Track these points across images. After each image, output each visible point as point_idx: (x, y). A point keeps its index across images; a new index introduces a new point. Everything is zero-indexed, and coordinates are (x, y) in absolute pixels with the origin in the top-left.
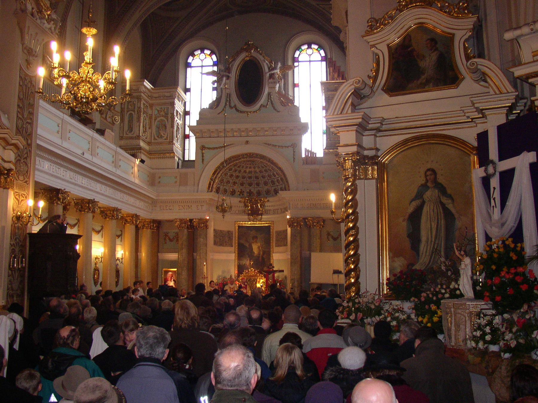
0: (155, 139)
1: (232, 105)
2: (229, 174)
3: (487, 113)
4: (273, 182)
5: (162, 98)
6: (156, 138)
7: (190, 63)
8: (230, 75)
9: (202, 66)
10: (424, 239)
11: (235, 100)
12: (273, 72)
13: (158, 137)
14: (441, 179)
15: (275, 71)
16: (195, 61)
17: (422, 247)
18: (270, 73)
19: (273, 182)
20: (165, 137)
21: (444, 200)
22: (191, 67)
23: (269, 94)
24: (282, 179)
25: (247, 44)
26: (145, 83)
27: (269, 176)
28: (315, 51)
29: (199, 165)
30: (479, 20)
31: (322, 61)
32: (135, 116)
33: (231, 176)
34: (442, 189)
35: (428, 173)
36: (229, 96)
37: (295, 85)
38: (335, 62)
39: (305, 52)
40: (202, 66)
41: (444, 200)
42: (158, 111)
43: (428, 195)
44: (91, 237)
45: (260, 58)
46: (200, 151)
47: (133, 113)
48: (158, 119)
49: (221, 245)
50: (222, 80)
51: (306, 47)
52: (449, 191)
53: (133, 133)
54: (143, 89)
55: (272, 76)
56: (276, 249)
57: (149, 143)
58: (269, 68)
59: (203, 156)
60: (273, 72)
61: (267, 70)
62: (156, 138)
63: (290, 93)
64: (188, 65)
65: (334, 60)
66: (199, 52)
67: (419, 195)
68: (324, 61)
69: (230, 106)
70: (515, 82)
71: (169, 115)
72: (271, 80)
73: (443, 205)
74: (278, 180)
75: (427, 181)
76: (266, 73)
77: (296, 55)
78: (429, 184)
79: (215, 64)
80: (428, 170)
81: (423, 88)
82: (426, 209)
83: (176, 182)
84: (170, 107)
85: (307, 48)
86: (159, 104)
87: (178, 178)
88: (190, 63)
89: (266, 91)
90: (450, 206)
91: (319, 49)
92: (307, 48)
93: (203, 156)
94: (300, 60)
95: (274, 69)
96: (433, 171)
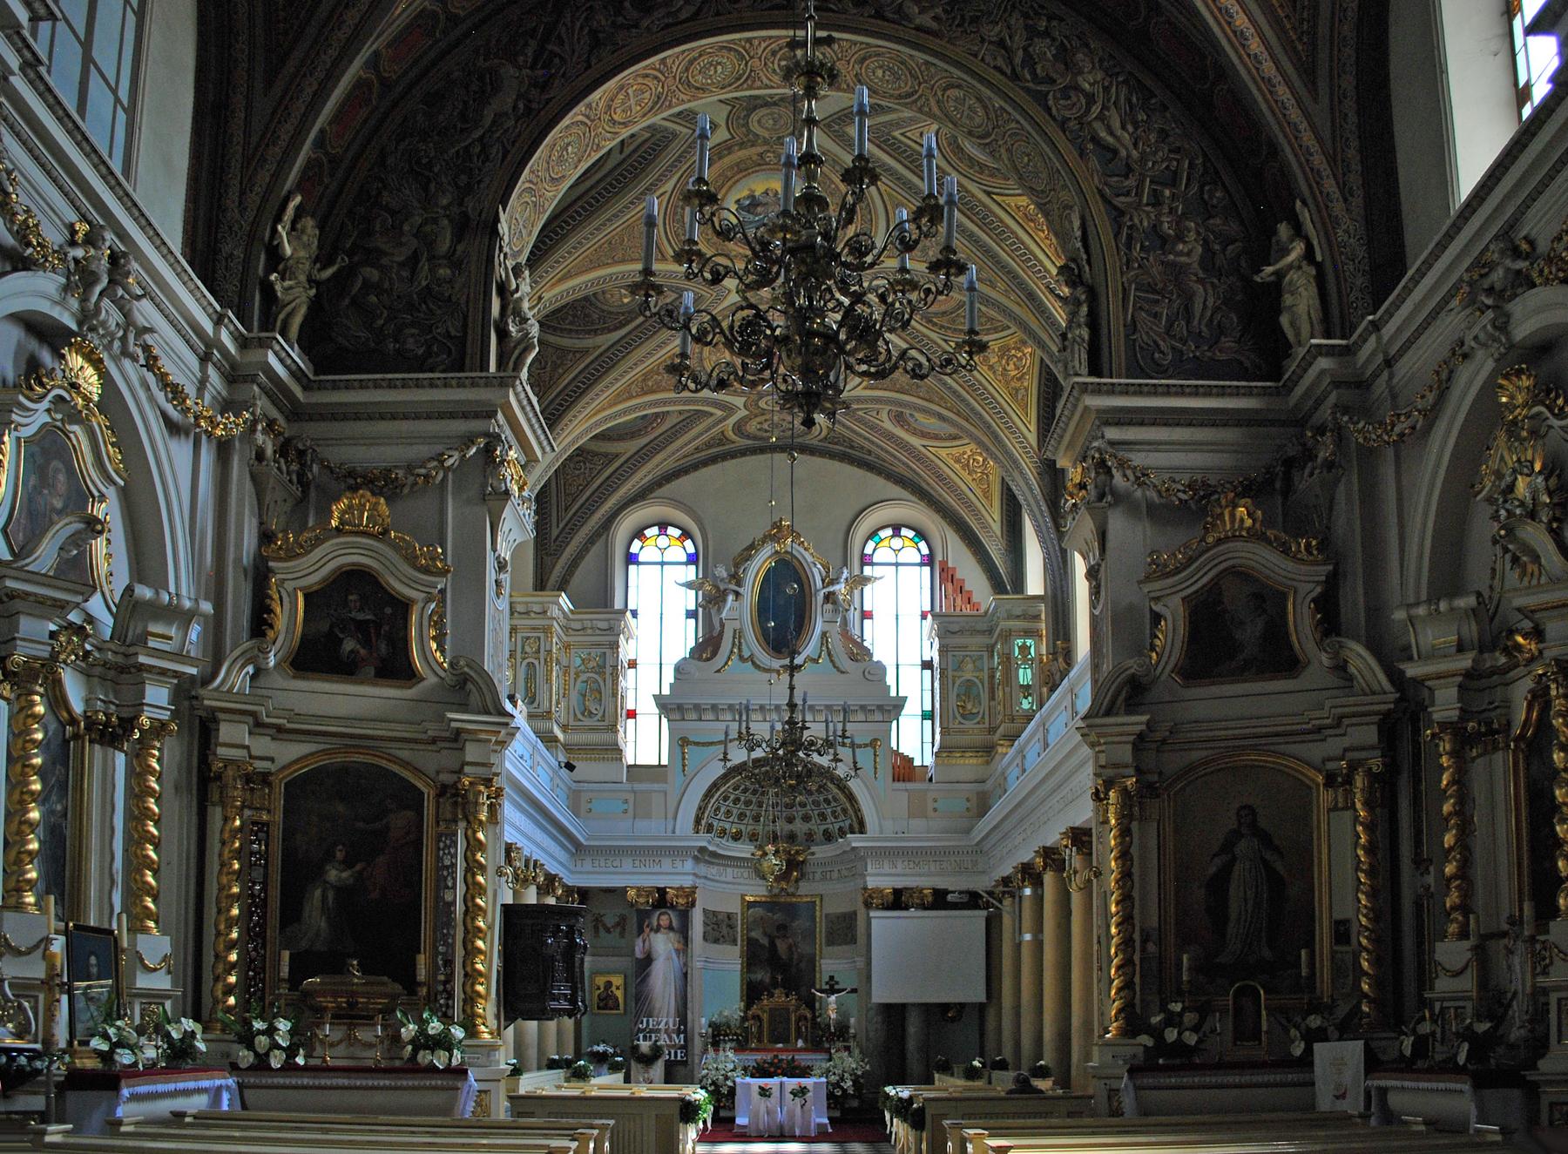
0: (576, 719)
1: (746, 654)
2: (732, 797)
3: (1499, 757)
4: (823, 816)
5: (589, 631)
6: (580, 716)
7: (636, 556)
8: (741, 590)
9: (662, 564)
10: (1233, 915)
11: (752, 643)
12: (831, 589)
13: (583, 714)
14: (1263, 823)
15: (836, 588)
16: (647, 551)
17: (1231, 929)
18: (826, 590)
19: (823, 816)
20: (598, 717)
21: (1268, 856)
22: (638, 563)
23: (824, 635)
24: (845, 811)
25: (777, 525)
26: (561, 600)
27: (813, 802)
28: (908, 543)
29: (676, 780)
30: (1336, 565)
31: (921, 564)
32: (540, 670)
33: (737, 800)
34: (1266, 839)
35: (1243, 813)
36: (738, 635)
37: (866, 615)
38: (954, 569)
39: (886, 543)
40: (662, 564)
41: (1268, 856)
42: (583, 660)
43: (1242, 847)
44: (527, 905)
45: (798, 551)
46: (678, 750)
47: (536, 662)
48: (583, 677)
49: (716, 941)
50: (725, 601)
51: (889, 532)
52: (1277, 842)
53: (535, 705)
54: (555, 612)
55: (829, 597)
56: (827, 950)
57: (564, 728)
58: (823, 581)
59: (684, 759)
60: (831, 589)
61: (819, 584)
62: (580, 716)
63: (857, 632)
64: (631, 559)
65: (950, 565)
66: (655, 530)
67: (1228, 846)
68: (925, 565)
69: (741, 657)
70: (1396, 677)
71: (608, 670)
72: (829, 606)
73: (1264, 861)
74: (834, 812)
75: (1240, 824)
76: (817, 591)
77: (868, 550)
78: (1244, 830)
79: (692, 559)
80: (1244, 807)
81: (1242, 672)
82: (1238, 868)
83: (625, 811)
84: (608, 652)
85: (892, 537)
86: (583, 645)
87: (930, 808)
88: (636, 556)
89: (819, 627)
90: (1279, 866)
91: (916, 540)
92: (892, 537)
93: (684, 759)
94: (875, 560)
95: (833, 582)
96: (1250, 809)
